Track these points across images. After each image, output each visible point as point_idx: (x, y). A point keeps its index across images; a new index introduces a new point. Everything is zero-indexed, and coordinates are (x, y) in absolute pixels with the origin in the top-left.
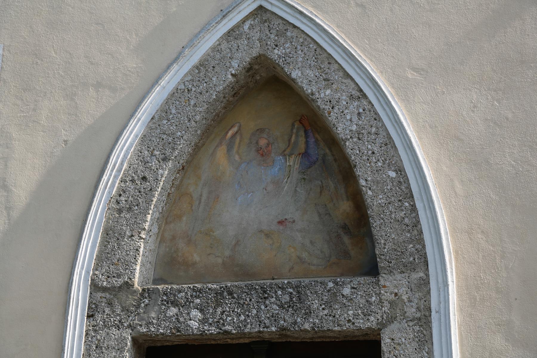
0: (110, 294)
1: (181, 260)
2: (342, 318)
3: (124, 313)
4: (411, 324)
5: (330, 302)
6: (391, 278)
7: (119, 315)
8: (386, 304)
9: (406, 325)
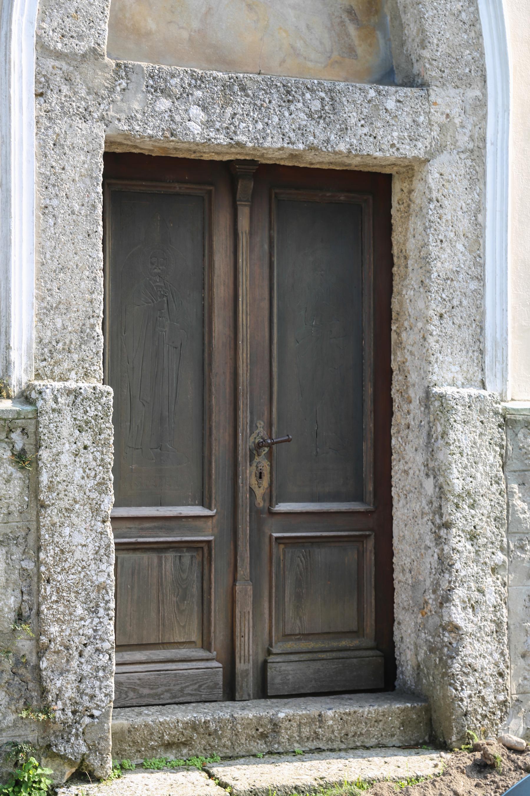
0: (69, 64)
1: (129, 25)
2: (385, 140)
3: (91, 96)
4: (463, 156)
5: (371, 117)
6: (443, 93)
7: (85, 99)
8: (436, 128)
9: (458, 156)
